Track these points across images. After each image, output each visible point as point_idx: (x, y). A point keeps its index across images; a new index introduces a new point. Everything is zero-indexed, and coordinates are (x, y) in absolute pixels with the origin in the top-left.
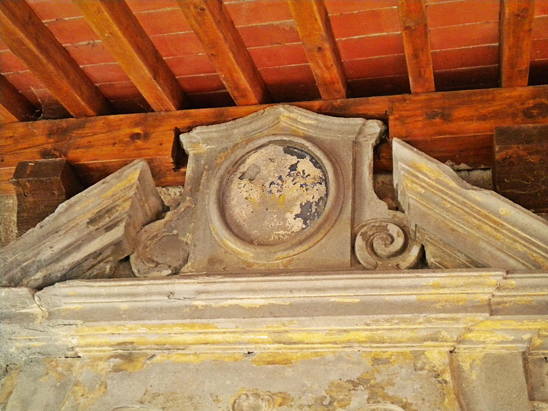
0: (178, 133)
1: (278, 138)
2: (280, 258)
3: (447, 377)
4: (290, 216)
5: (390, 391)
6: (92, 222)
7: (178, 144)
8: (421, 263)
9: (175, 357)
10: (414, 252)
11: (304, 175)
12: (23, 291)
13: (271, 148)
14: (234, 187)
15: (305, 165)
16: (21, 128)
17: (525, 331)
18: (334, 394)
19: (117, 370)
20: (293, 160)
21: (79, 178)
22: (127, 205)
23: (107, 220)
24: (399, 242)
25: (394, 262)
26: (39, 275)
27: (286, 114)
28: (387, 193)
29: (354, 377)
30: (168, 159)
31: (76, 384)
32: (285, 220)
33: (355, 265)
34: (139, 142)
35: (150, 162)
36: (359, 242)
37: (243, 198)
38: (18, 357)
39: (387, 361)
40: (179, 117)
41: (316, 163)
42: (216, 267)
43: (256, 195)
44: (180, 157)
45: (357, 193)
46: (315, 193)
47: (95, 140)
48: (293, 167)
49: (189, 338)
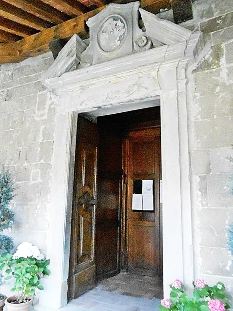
0: (85, 21)
1: (111, 16)
2: (114, 54)
3: (156, 78)
4: (116, 41)
5: (142, 85)
6: (67, 56)
7: (86, 25)
8: (152, 46)
9: (93, 86)
10: (150, 43)
11: (119, 26)
12: (56, 78)
13: (110, 19)
14: (101, 35)
15: (119, 23)
16: (47, 30)
17: (176, 62)
18: (130, 88)
19: (81, 92)
20: (116, 22)
21: (63, 42)
22: (75, 48)
23: (71, 54)
24: (145, 41)
25: (144, 49)
26: (59, 73)
27: (112, 6)
28: (141, 26)
29: (134, 83)
30: (83, 30)
31: (74, 97)
32: (115, 42)
33: (134, 52)
34: (76, 27)
35: (78, 34)
36: (135, 44)
37: (103, 38)
38: (11, 164)
39: (142, 77)
40: (83, 16)
41: (122, 22)
42: (100, 61)
43: (107, 36)
44: (87, 29)
45: (190, 133)
46: (122, 33)
47: (66, 27)
48: (116, 25)
49: (96, 82)
